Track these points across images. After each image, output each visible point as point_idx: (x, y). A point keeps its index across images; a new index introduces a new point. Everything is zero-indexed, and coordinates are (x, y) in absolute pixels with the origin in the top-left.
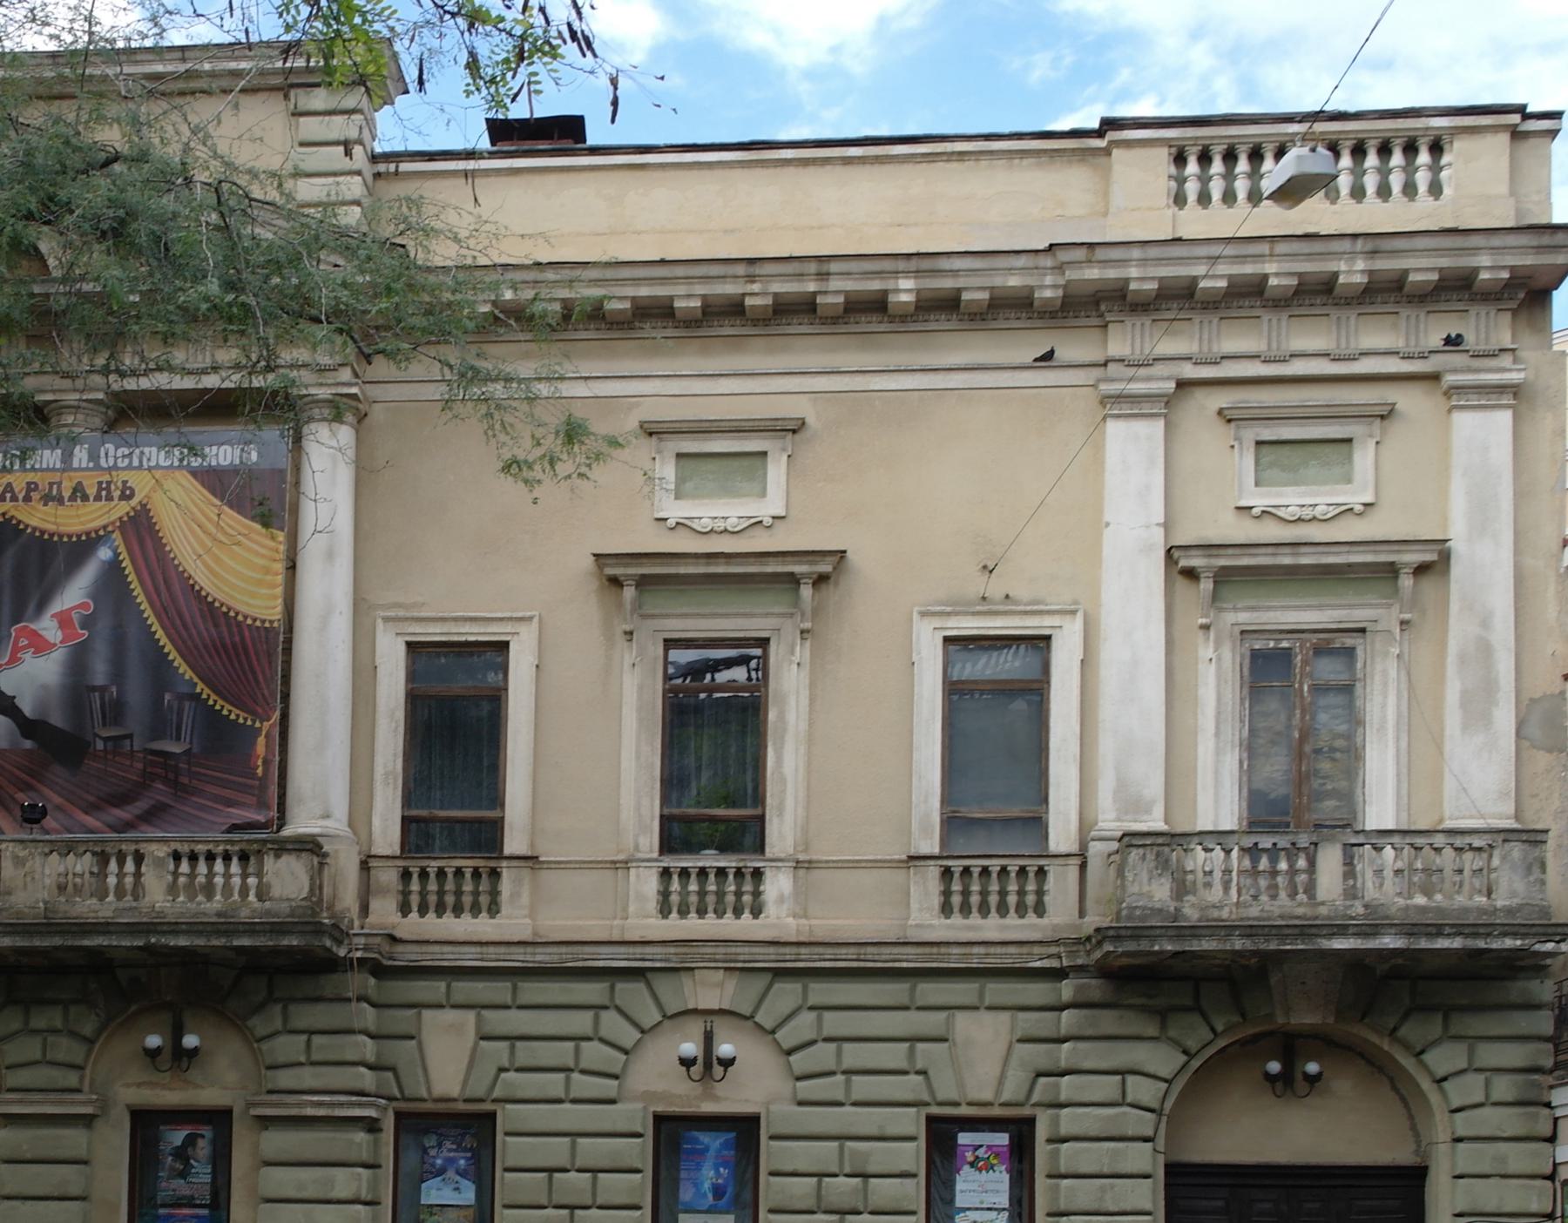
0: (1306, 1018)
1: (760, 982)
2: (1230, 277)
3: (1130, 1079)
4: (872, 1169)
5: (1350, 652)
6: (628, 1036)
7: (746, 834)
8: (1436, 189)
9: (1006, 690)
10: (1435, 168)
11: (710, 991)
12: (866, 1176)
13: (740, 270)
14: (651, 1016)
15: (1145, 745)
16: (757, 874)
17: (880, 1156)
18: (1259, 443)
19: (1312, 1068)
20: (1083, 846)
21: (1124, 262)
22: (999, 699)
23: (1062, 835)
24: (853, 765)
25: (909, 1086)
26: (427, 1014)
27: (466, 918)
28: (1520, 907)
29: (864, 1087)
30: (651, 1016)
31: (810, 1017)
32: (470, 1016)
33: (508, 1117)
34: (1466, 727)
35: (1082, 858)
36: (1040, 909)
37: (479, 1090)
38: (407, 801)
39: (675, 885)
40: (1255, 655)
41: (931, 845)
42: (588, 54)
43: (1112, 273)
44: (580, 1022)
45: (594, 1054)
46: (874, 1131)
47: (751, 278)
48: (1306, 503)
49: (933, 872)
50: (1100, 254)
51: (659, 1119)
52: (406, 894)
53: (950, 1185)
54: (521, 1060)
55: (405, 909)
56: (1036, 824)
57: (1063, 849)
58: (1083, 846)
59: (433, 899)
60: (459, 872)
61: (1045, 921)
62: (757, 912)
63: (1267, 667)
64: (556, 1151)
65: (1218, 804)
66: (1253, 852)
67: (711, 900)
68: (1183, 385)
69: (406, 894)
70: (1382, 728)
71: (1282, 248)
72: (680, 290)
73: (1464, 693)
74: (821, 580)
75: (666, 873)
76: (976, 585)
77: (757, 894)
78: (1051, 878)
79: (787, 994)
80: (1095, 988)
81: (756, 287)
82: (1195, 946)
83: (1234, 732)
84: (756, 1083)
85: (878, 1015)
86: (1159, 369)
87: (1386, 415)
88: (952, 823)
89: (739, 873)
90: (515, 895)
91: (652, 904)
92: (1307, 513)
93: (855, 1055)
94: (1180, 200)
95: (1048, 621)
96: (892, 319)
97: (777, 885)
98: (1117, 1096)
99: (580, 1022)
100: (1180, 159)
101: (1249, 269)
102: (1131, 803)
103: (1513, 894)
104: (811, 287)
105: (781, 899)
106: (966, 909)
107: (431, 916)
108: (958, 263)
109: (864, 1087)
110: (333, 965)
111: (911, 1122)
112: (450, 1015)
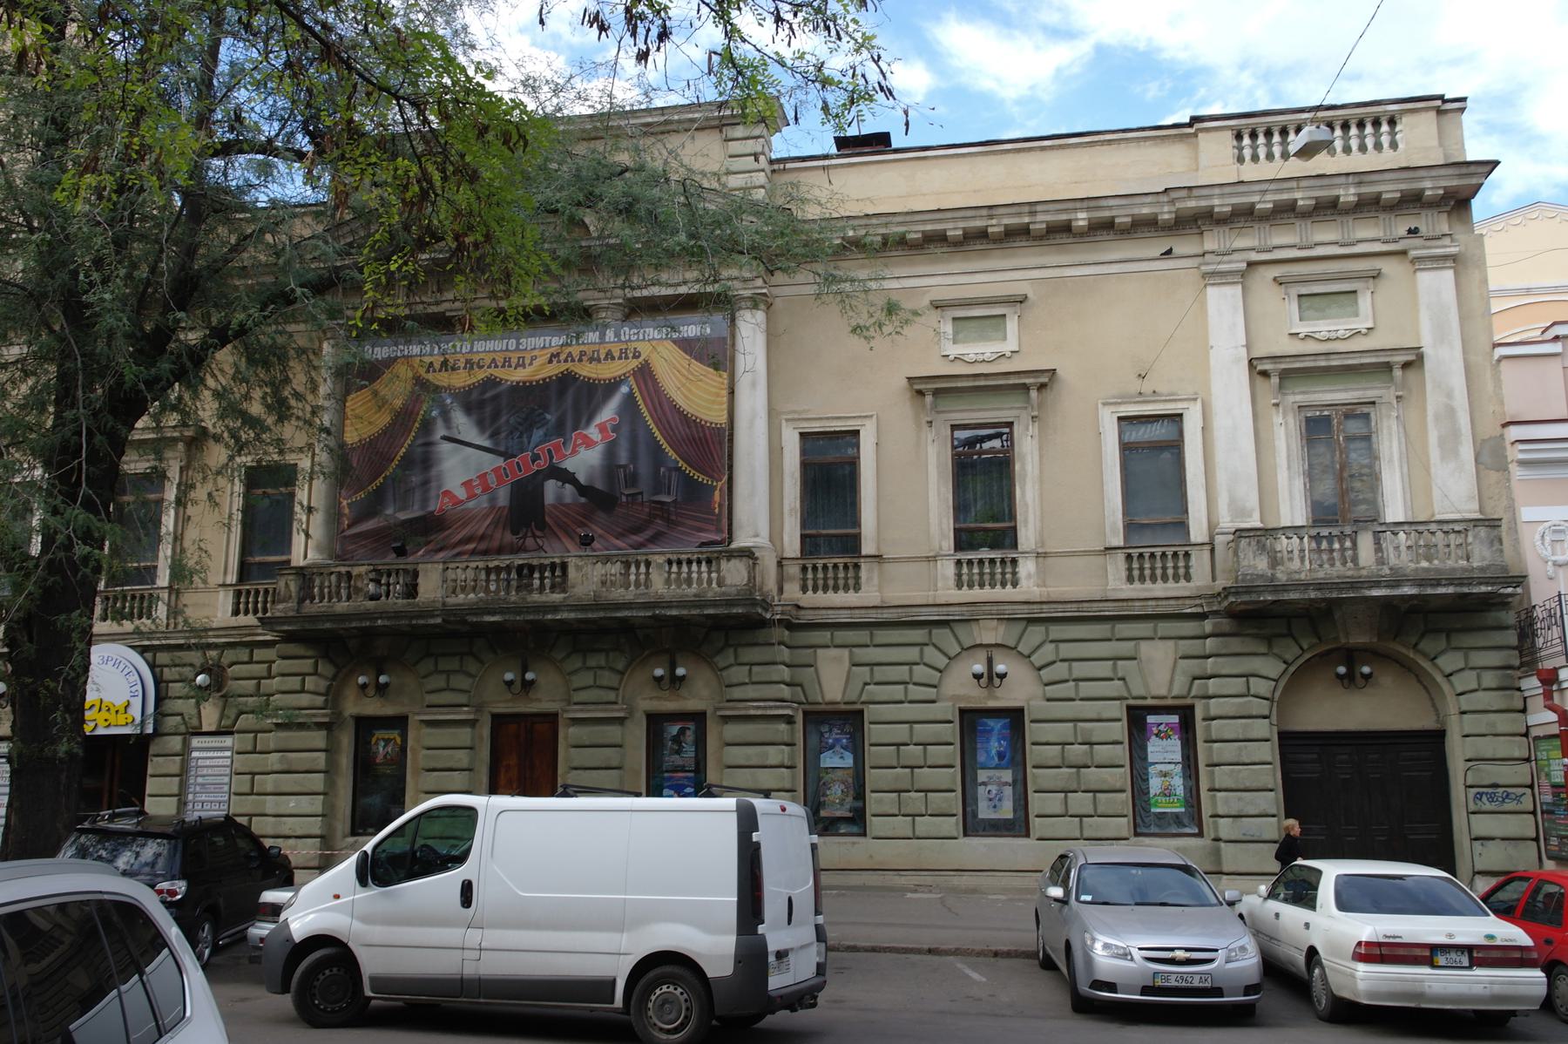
0: (1359, 638)
1: (1020, 626)
2: (1047, 222)
3: (1252, 680)
4: (1094, 739)
5: (1367, 416)
6: (941, 661)
7: (1006, 538)
8: (1394, 145)
9: (1157, 447)
10: (1393, 133)
11: (989, 633)
12: (1091, 744)
13: (984, 212)
14: (954, 649)
15: (1245, 475)
16: (1014, 561)
17: (1099, 731)
19: (1366, 670)
20: (1212, 538)
23: (1198, 532)
24: (1069, 495)
25: (1115, 688)
28: (1488, 567)
29: (1087, 689)
30: (954, 649)
32: (846, 652)
33: (871, 712)
34: (1443, 458)
35: (1211, 545)
36: (1188, 577)
37: (853, 697)
38: (803, 525)
39: (965, 570)
40: (1308, 420)
41: (1118, 541)
43: (1203, 203)
44: (912, 654)
45: (921, 672)
46: (1094, 716)
47: (991, 217)
48: (1331, 329)
50: (994, 212)
51: (962, 712)
52: (804, 580)
53: (1144, 748)
54: (878, 678)
56: (1182, 526)
57: (1199, 540)
58: (1212, 538)
61: (1191, 584)
62: (1015, 584)
63: (1316, 427)
64: (901, 732)
65: (1293, 509)
66: (1317, 538)
69: (804, 580)
70: (1391, 461)
71: (1304, 183)
72: (950, 225)
73: (1440, 438)
75: (959, 563)
76: (1135, 386)
79: (1036, 634)
80: (1226, 624)
81: (994, 222)
82: (1286, 596)
84: (1020, 688)
85: (1094, 645)
86: (1236, 256)
87: (1376, 276)
88: (1130, 527)
89: (1003, 561)
90: (869, 579)
91: (952, 582)
93: (1080, 669)
94: (1241, 159)
97: (1026, 568)
99: (912, 654)
100: (1239, 137)
101: (1285, 196)
102: (1238, 511)
103: (1484, 559)
104: (1026, 220)
105: (1029, 576)
106: (1142, 579)
107: (820, 592)
108: (1112, 202)
109: (1087, 689)
110: (763, 624)
111: (1117, 709)
112: (833, 652)
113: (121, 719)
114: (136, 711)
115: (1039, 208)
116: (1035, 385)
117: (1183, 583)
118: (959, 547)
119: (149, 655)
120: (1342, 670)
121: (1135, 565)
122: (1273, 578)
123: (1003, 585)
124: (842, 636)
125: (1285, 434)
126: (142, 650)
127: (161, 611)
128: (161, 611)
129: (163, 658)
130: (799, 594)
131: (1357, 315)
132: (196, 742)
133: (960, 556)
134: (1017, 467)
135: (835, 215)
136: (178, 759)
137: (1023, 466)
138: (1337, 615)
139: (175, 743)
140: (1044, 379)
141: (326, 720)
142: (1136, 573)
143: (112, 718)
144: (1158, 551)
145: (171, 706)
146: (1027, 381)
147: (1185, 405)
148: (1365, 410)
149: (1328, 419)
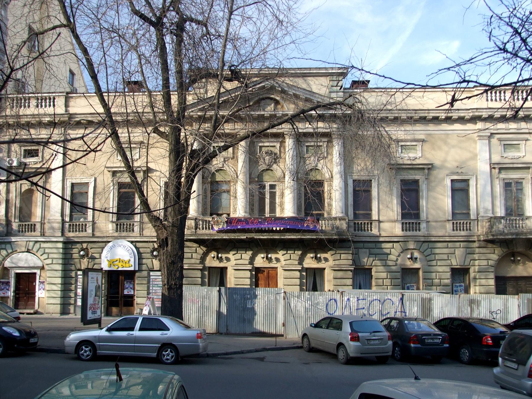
0: (520, 249)
1: (421, 243)
5: (522, 183)
7: (417, 216)
9: (462, 190)
13: (414, 112)
16: (419, 223)
18: (504, 145)
19: (519, 258)
21: (482, 112)
22: (460, 190)
24: (437, 202)
26: (360, 250)
27: (363, 232)
31: (430, 250)
32: (368, 250)
40: (506, 183)
41: (450, 218)
42: (52, 107)
47: (416, 113)
49: (451, 223)
50: (478, 110)
51: (403, 269)
52: (355, 227)
55: (355, 230)
56: (468, 214)
57: (474, 219)
58: (478, 218)
59: (408, 228)
60: (413, 223)
62: (419, 230)
63: (507, 185)
65: (500, 212)
67: (411, 228)
68: (492, 134)
69: (355, 227)
70: (529, 196)
74: (429, 169)
75: (403, 223)
77: (419, 227)
78: (472, 223)
80: (483, 244)
81: (417, 115)
82: (507, 237)
83: (503, 198)
86: (487, 131)
87: (527, 140)
88: (453, 214)
89: (416, 223)
92: (513, 157)
95: (469, 177)
96: (439, 121)
97: (423, 225)
98: (240, 258)
102: (486, 210)
105: (424, 228)
106: (457, 230)
112: (364, 250)
113: (127, 265)
114: (132, 262)
115: (431, 112)
116: (428, 168)
117: (468, 231)
118: (402, 218)
119: (134, 244)
120: (512, 259)
121: (404, 226)
122: (504, 232)
123: (413, 231)
124: (366, 245)
125: (498, 188)
126: (132, 242)
127: (89, 230)
128: (89, 230)
129: (139, 245)
130: (354, 232)
131: (519, 152)
132: (152, 273)
133: (404, 221)
134: (421, 194)
135: (147, 83)
136: (146, 279)
137: (423, 194)
138: (514, 242)
139: (145, 273)
140: (430, 167)
141: (201, 268)
142: (455, 228)
143: (124, 265)
144: (78, 223)
145: (144, 261)
146: (425, 167)
147: (470, 177)
148: (520, 181)
149: (511, 183)
